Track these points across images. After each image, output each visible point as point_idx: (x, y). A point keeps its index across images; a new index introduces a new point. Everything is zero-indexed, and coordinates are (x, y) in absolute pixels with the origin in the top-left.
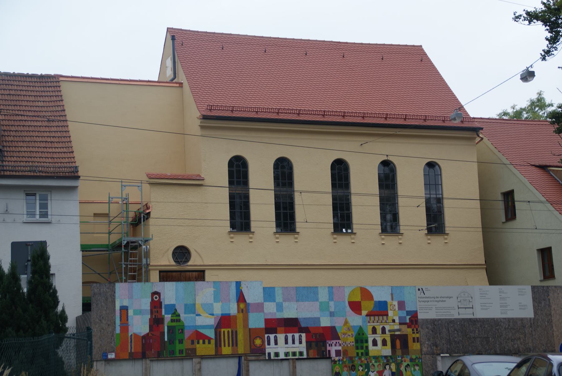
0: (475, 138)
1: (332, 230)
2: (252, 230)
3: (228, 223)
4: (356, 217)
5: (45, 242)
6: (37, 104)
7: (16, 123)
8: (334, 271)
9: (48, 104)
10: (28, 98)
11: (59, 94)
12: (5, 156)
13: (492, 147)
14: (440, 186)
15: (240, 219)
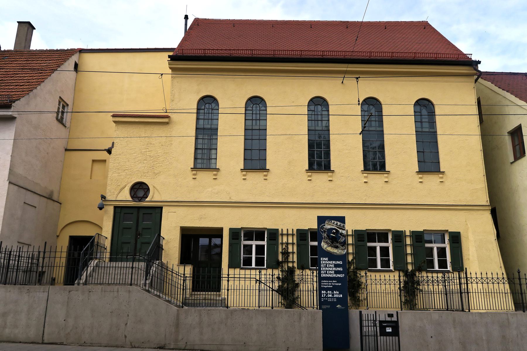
1: (307, 167)
4: (272, 159)
5: (344, 217)
15: (204, 157)
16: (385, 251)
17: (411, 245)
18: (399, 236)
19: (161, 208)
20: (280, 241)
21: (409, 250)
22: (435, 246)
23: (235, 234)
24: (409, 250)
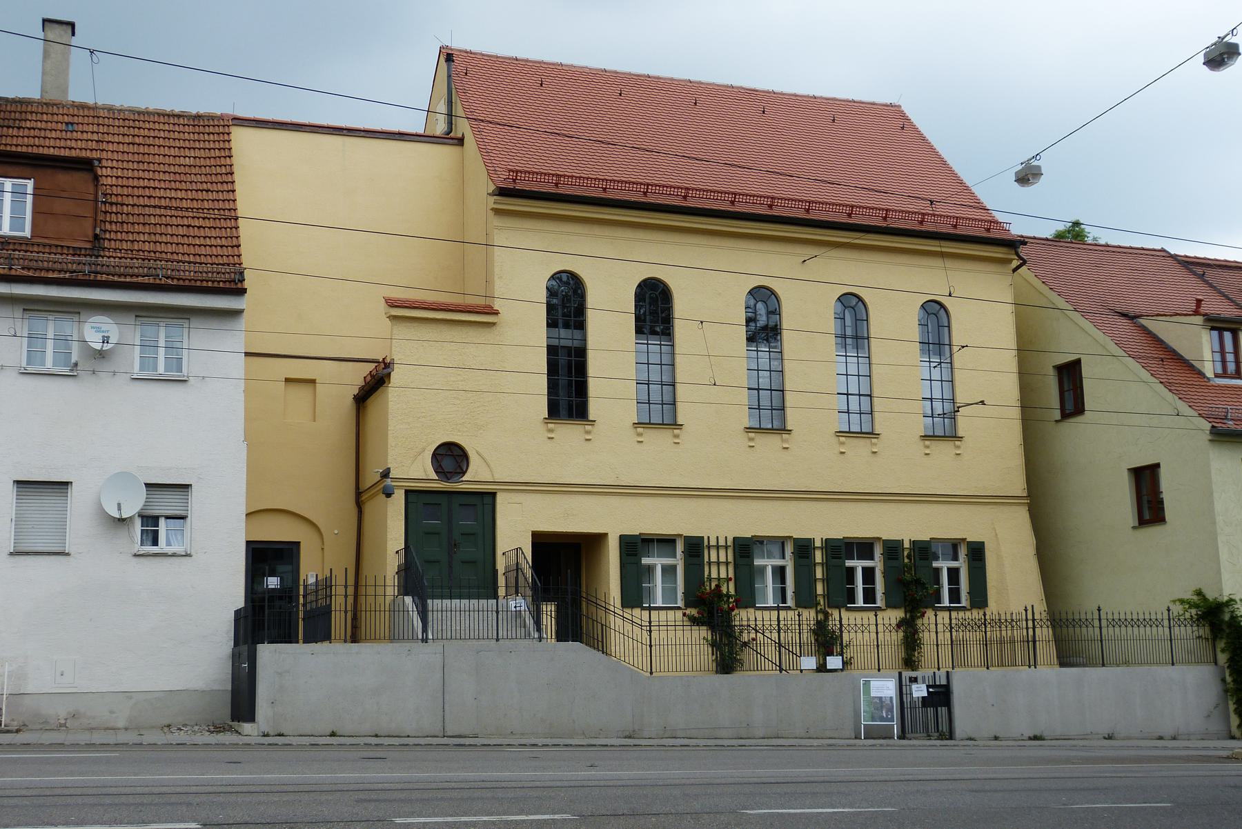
0: (1010, 261)
2: (591, 418)
3: (544, 401)
5: (983, 543)
6: (182, 161)
7: (136, 192)
8: (749, 502)
9: (203, 162)
10: (167, 151)
11: (227, 145)
12: (104, 249)
13: (1037, 283)
14: (947, 347)
15: (568, 393)
16: (869, 574)
17: (822, 564)
18: (803, 549)
19: (493, 495)
20: (706, 559)
21: (819, 573)
22: (944, 565)
23: (633, 547)
24: (819, 573)
